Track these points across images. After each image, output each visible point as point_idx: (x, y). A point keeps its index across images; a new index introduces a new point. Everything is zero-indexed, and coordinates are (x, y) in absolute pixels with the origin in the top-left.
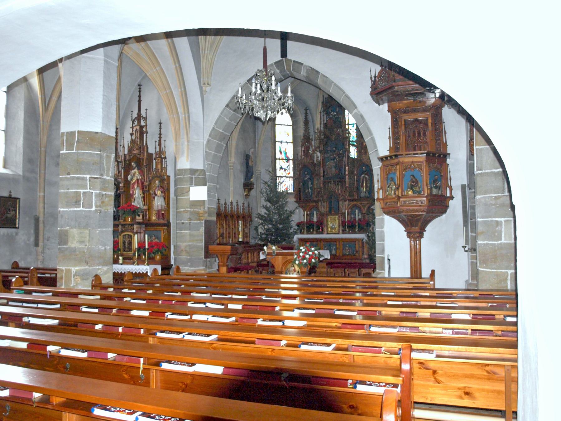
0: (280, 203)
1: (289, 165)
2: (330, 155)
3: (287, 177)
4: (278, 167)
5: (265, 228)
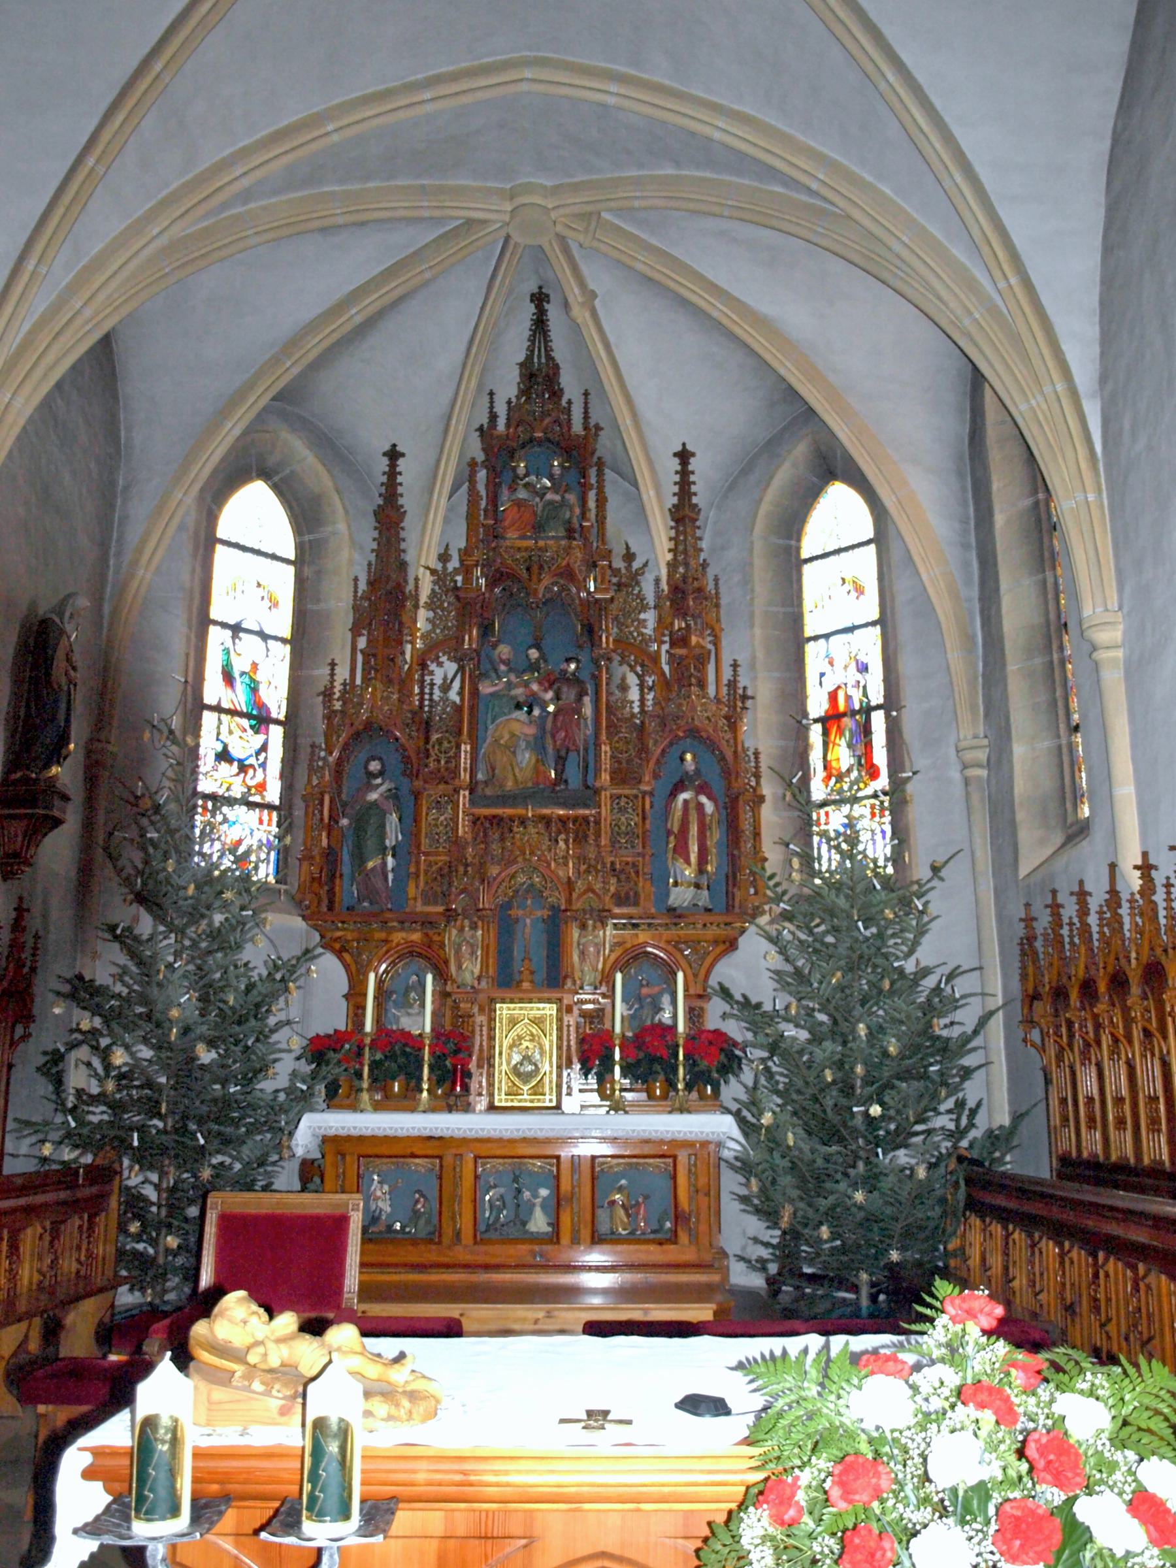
1: (264, 748)
3: (252, 805)
4: (208, 746)
5: (108, 1067)
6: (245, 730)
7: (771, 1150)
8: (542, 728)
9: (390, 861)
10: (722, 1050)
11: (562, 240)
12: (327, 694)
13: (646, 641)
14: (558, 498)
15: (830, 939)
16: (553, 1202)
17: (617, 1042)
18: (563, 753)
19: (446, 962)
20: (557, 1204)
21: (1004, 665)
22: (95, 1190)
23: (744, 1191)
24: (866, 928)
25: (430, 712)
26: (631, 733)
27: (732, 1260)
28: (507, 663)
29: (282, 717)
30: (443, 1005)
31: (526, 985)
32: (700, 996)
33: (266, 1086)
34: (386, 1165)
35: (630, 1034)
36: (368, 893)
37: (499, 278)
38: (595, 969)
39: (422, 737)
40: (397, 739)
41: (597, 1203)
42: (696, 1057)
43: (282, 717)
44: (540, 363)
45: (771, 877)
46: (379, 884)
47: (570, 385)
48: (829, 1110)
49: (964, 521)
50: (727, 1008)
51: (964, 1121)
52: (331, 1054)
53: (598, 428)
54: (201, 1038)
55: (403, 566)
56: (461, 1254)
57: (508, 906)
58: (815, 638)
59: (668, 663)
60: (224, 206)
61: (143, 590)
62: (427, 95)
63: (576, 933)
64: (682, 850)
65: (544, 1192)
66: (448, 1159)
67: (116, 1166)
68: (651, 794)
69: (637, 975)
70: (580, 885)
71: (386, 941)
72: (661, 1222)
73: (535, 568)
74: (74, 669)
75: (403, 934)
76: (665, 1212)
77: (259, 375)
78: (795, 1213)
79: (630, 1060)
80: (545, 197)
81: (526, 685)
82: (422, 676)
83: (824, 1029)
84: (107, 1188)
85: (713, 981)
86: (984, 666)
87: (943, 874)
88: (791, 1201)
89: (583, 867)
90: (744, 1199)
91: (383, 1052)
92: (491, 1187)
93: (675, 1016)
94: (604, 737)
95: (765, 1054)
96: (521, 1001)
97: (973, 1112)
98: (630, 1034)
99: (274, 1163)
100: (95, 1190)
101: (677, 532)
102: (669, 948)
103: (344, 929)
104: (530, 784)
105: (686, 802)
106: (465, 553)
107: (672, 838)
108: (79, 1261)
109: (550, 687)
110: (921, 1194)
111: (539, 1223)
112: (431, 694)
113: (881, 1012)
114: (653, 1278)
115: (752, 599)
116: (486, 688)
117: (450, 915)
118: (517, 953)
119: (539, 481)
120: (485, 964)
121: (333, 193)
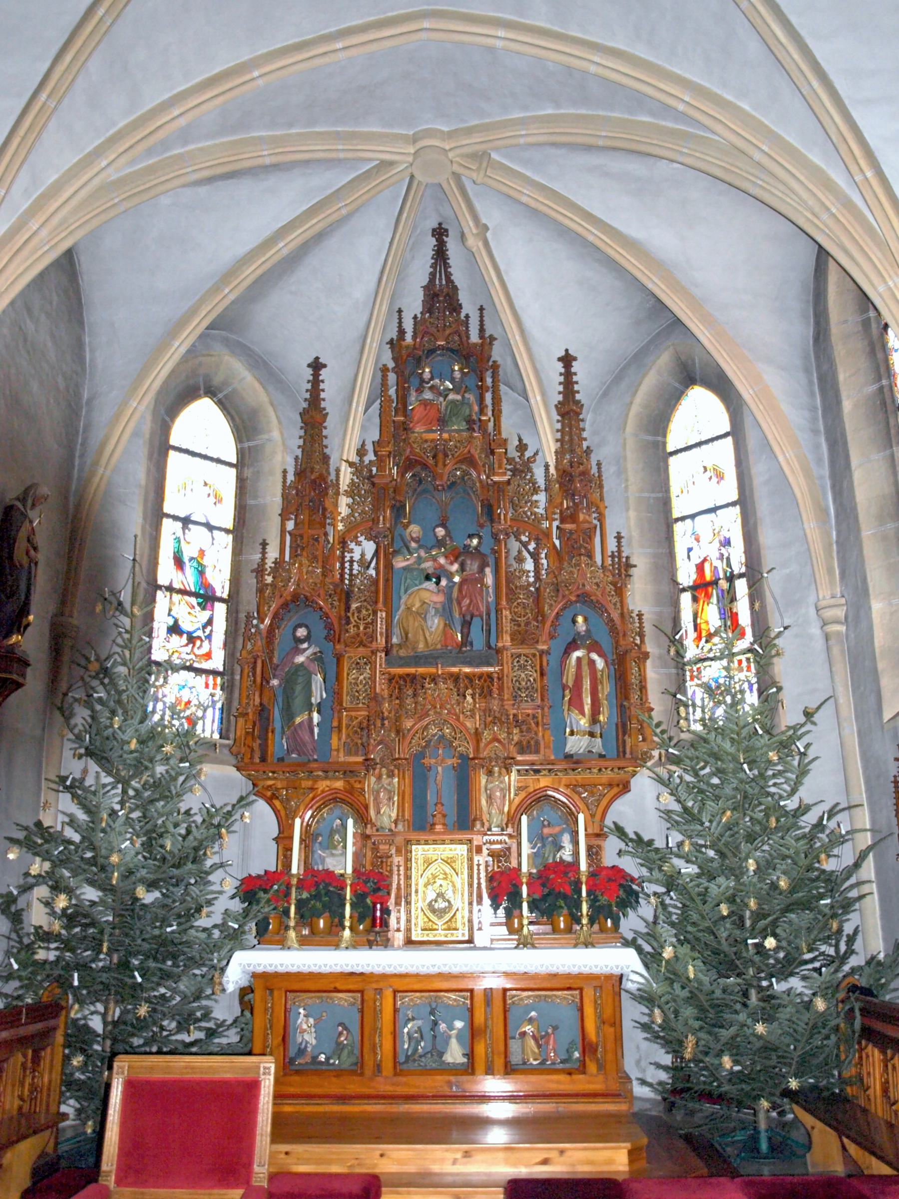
0: (160, 769)
1: (210, 622)
2: (420, 560)
3: (199, 671)
6: (193, 607)
7: (672, 982)
8: (449, 599)
9: (316, 717)
10: (621, 885)
11: (457, 177)
12: (260, 571)
13: (538, 519)
14: (459, 397)
15: (715, 781)
16: (467, 1035)
17: (524, 880)
18: (468, 618)
19: (367, 807)
20: (473, 1033)
21: (858, 531)
22: (39, 1026)
23: (645, 1019)
24: (750, 770)
25: (351, 585)
26: (528, 598)
27: (635, 1083)
28: (417, 540)
29: (225, 596)
30: (365, 846)
31: (439, 828)
32: (598, 835)
33: (203, 922)
34: (311, 999)
35: (534, 871)
36: (297, 745)
37: (405, 215)
38: (501, 812)
39: (343, 607)
40: (321, 609)
41: (509, 1034)
42: (598, 893)
43: (225, 596)
44: (441, 285)
45: (658, 725)
46: (307, 738)
47: (468, 306)
48: (723, 941)
49: (813, 409)
50: (622, 845)
51: (843, 947)
52: (261, 894)
53: (492, 339)
54: (142, 881)
55: (326, 459)
56: (383, 1086)
57: (422, 755)
58: (683, 519)
59: (559, 538)
60: (165, 145)
61: (103, 486)
62: (339, 45)
63: (483, 780)
64: (576, 703)
65: (459, 1024)
66: (369, 994)
67: (63, 1003)
68: (548, 652)
69: (539, 816)
70: (486, 735)
71: (312, 789)
72: (569, 1052)
73: (441, 456)
74: (35, 549)
75: (328, 783)
76: (572, 1043)
77: (203, 300)
78: (697, 1042)
79: (536, 896)
80: (444, 140)
81: (434, 559)
82: (343, 553)
83: (715, 865)
84: (52, 1023)
85: (608, 822)
86: (838, 536)
87: (816, 718)
88: (694, 1032)
89: (489, 719)
90: (645, 1027)
91: (309, 892)
92: (409, 1020)
93: (576, 854)
94: (504, 603)
95: (662, 890)
96: (435, 842)
97: (851, 940)
98: (534, 871)
99: (208, 997)
100: (39, 1026)
101: (563, 426)
102: (568, 792)
103: (275, 779)
104: (439, 646)
105: (579, 659)
106: (377, 445)
107: (567, 692)
108: (21, 1098)
109: (456, 560)
110: (819, 1024)
111: (455, 1054)
112: (351, 570)
113: (766, 847)
114: (564, 1107)
115: (626, 487)
116: (399, 563)
117: (369, 765)
118: (431, 797)
119: (442, 383)
120: (401, 808)
121: (260, 138)
